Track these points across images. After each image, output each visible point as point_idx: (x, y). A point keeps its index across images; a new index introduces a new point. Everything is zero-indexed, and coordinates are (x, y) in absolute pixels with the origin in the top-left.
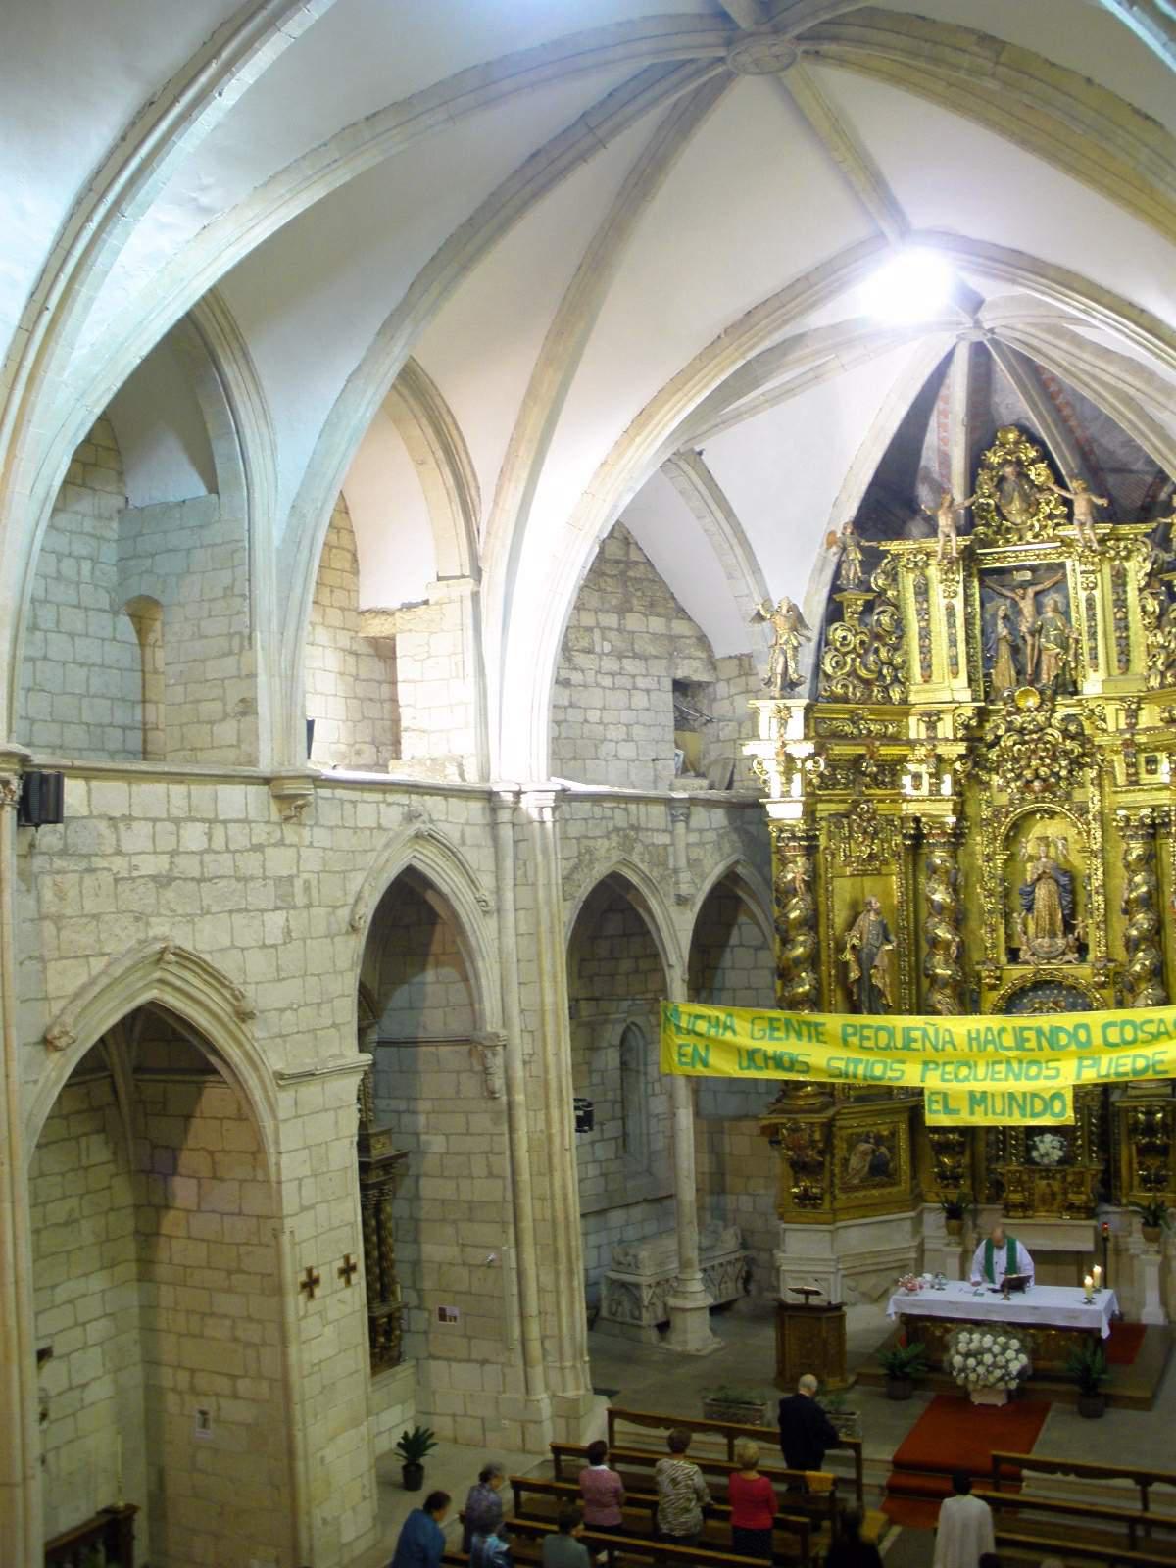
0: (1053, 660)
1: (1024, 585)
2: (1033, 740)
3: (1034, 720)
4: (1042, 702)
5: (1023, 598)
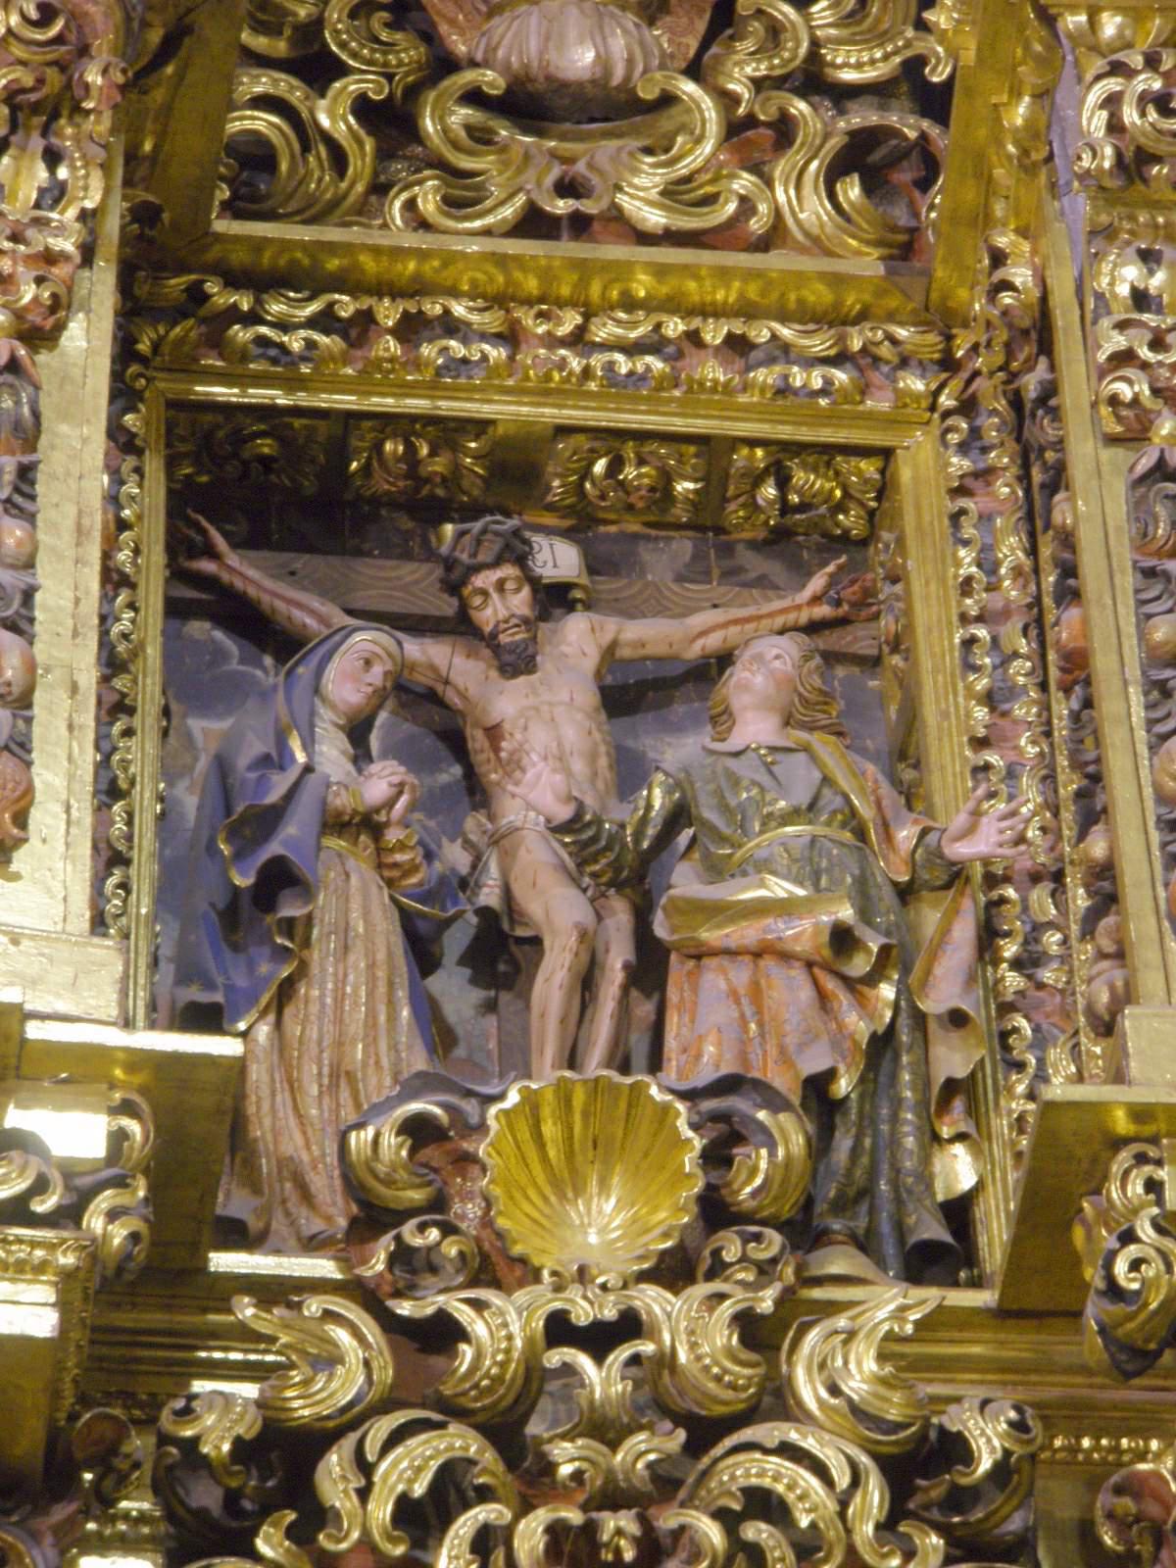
0: (792, 991)
1: (554, 599)
2: (613, 1497)
3: (630, 1325)
4: (715, 1211)
5: (517, 662)
